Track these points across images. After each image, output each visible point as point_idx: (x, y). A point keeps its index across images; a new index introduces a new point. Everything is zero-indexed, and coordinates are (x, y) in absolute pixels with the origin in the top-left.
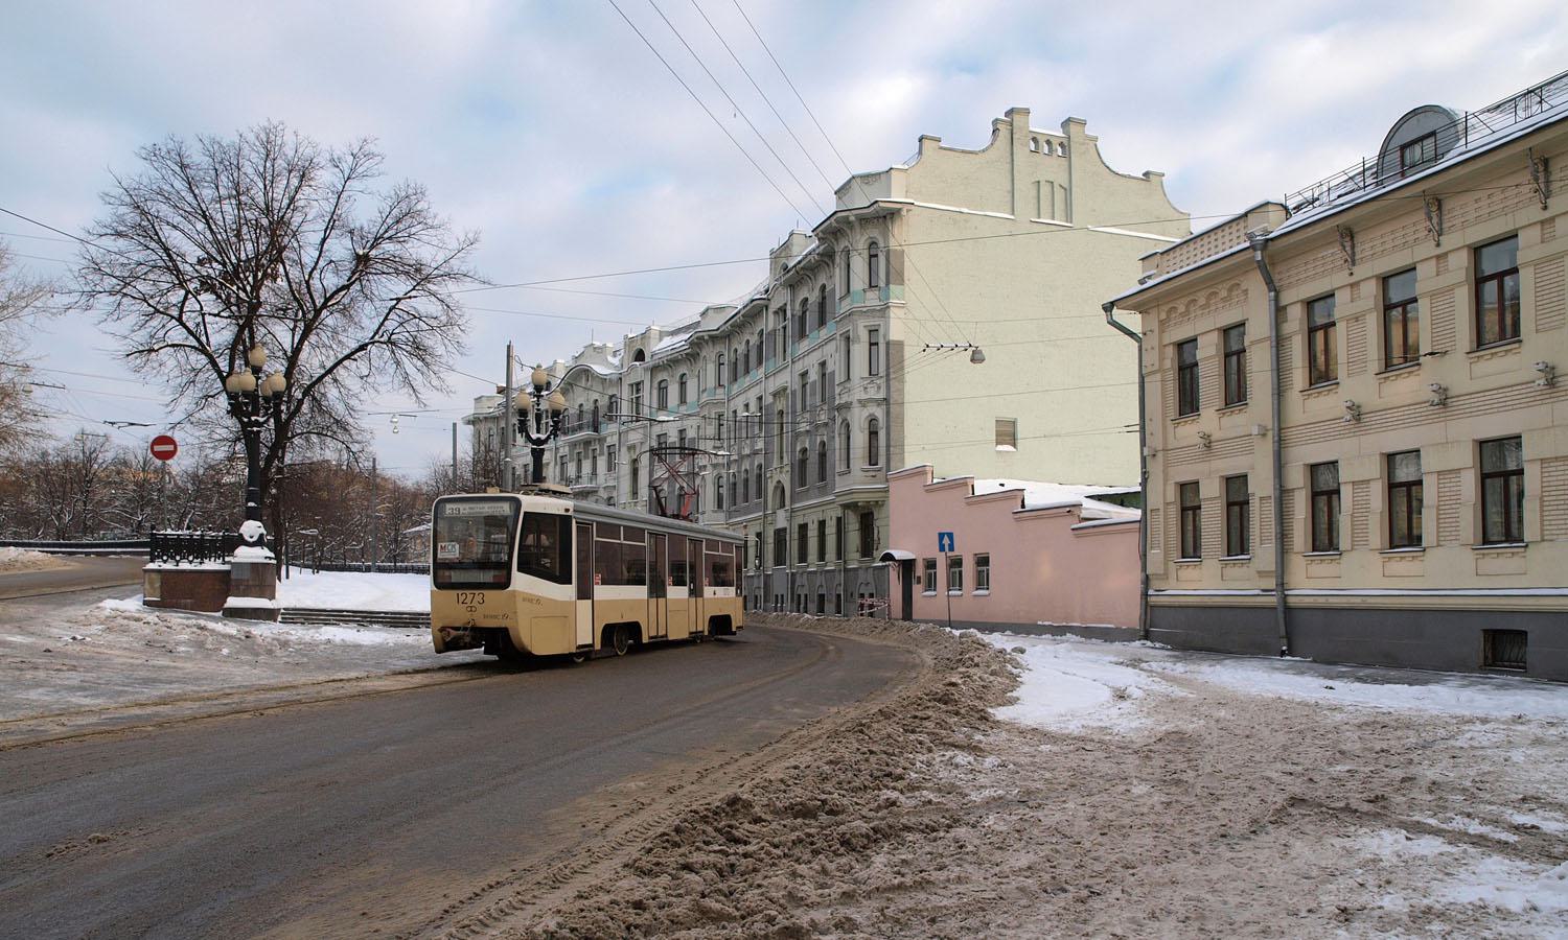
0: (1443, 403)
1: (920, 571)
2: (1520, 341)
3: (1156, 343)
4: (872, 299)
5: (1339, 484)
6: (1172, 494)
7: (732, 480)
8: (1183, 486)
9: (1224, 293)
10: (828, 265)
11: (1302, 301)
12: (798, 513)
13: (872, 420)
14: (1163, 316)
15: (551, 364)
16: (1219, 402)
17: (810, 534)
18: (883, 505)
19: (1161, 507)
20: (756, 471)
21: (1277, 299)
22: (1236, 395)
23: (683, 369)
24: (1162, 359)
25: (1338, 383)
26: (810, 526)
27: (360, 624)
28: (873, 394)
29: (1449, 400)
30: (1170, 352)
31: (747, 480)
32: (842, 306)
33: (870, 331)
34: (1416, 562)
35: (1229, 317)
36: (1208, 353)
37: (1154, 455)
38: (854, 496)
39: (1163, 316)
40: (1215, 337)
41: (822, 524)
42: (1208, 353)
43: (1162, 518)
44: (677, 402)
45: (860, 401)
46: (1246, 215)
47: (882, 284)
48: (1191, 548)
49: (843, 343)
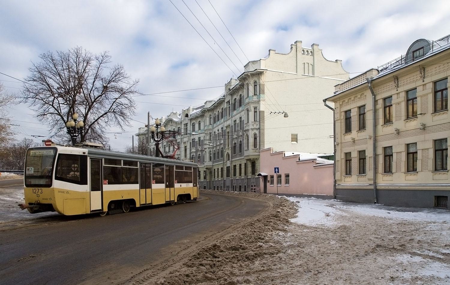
0: (424, 129)
1: (269, 179)
4: (255, 98)
5: (392, 153)
9: (359, 96)
10: (242, 88)
13: (255, 134)
14: (341, 103)
16: (357, 129)
18: (258, 159)
21: (375, 98)
22: (362, 126)
24: (340, 116)
25: (393, 123)
28: (255, 126)
30: (343, 114)
33: (254, 108)
36: (354, 114)
38: (250, 157)
40: (356, 109)
41: (240, 165)
42: (354, 114)
43: (340, 163)
45: (251, 129)
46: (366, 73)
47: (258, 94)
49: (246, 112)
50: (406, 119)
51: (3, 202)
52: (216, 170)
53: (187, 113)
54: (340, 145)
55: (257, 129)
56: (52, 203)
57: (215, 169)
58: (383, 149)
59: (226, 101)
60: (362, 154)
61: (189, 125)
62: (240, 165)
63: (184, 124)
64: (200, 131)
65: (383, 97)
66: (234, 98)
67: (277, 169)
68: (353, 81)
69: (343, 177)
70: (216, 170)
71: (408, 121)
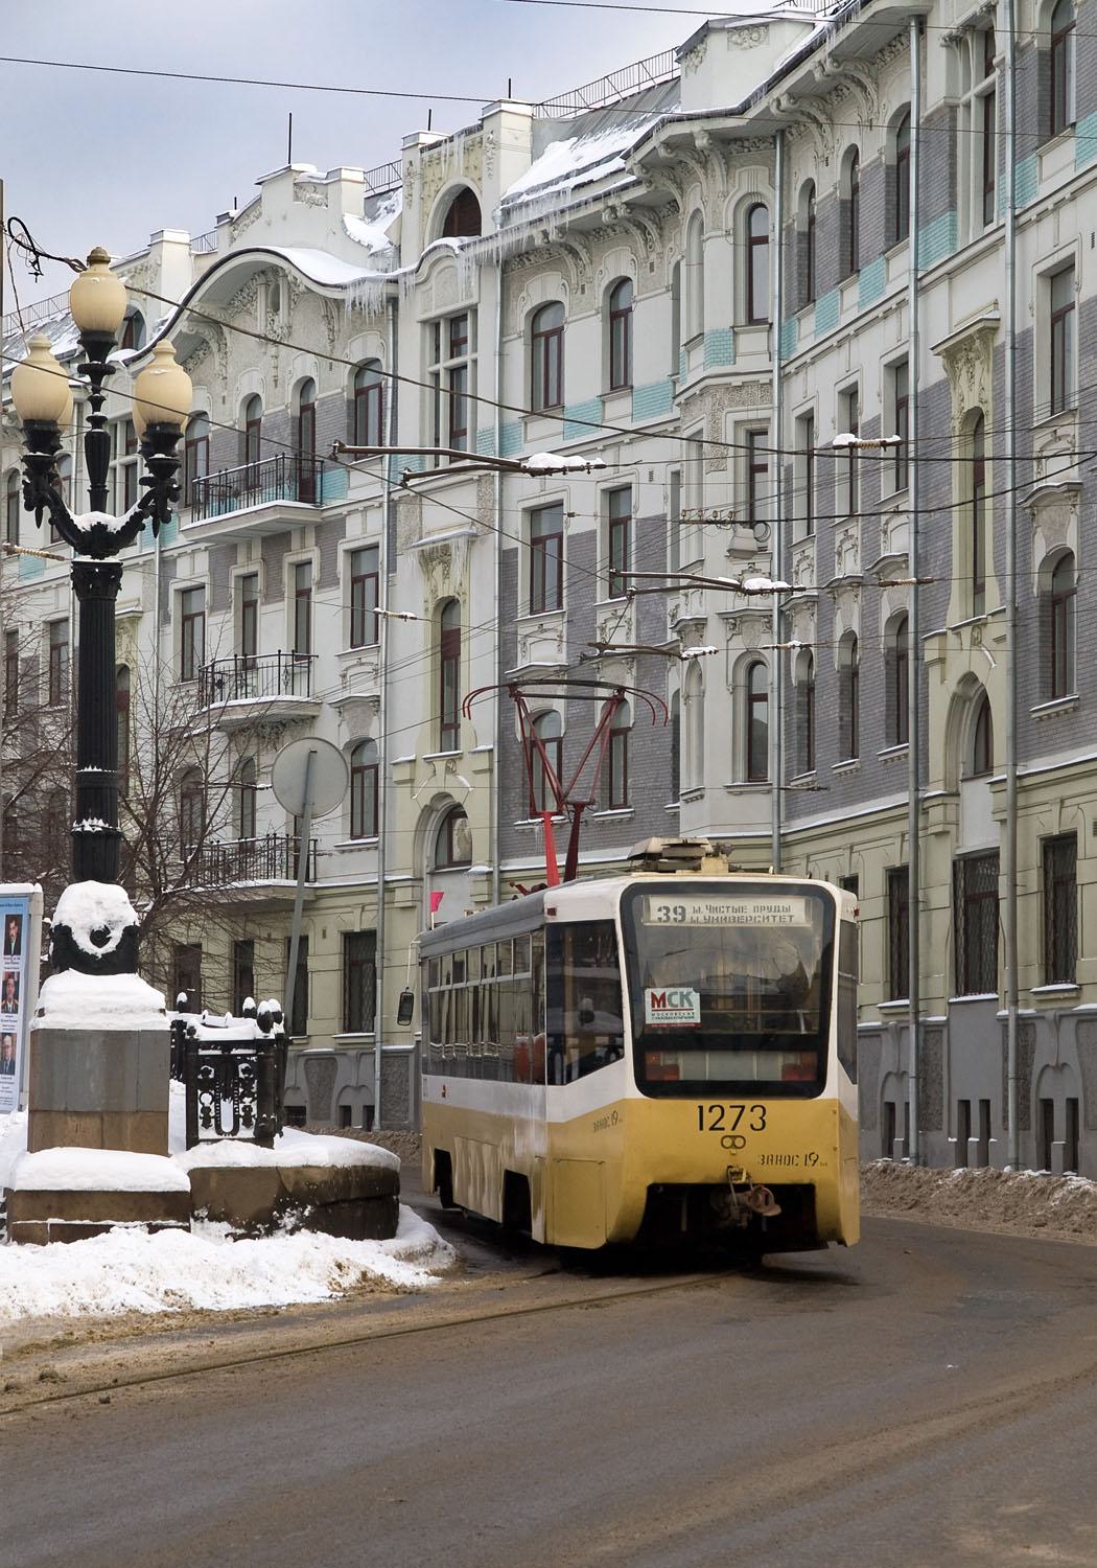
7: (797, 672)
20: (884, 640)
31: (851, 675)
45: (724, 616)
53: (455, 176)
63: (433, 325)
64: (620, 412)
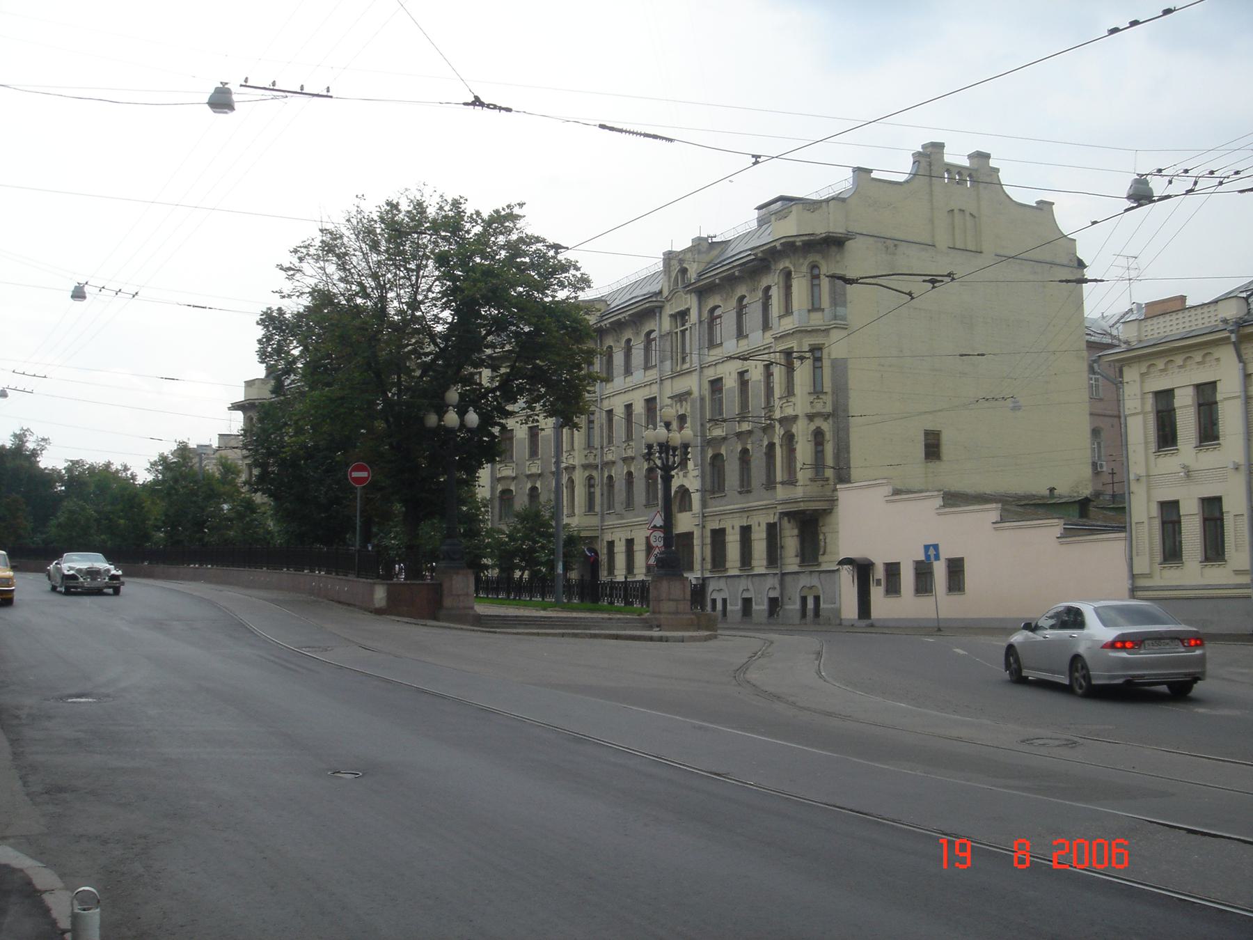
0: (1237, 469)
1: (880, 573)
2: (1219, 444)
3: (1138, 392)
5: (1180, 516)
6: (1155, 511)
8: (1163, 505)
9: (1199, 359)
11: (1193, 385)
12: (605, 531)
14: (1144, 370)
15: (522, 215)
16: (1194, 441)
17: (754, 536)
18: (831, 512)
19: (1146, 521)
21: (1245, 369)
22: (1208, 433)
23: (742, 290)
24: (1143, 404)
25: (1177, 449)
26: (755, 528)
27: (605, 125)
29: (1190, 473)
30: (1150, 401)
32: (607, 387)
34: (1221, 567)
35: (1203, 377)
36: (1185, 403)
37: (1138, 480)
39: (1144, 370)
40: (1190, 391)
41: (746, 531)
42: (1185, 403)
43: (1146, 529)
44: (806, 305)
46: (1216, 302)
48: (1172, 553)
50: (1198, 444)
51: (1142, 652)
52: (620, 548)
54: (1144, 479)
55: (826, 417)
56: (876, 563)
57: (611, 544)
58: (1201, 501)
59: (670, 309)
60: (1212, 508)
61: (694, 316)
62: (746, 531)
65: (1195, 383)
66: (626, 338)
67: (931, 548)
68: (1171, 318)
69: (1157, 567)
70: (620, 548)
71: (1216, 448)
